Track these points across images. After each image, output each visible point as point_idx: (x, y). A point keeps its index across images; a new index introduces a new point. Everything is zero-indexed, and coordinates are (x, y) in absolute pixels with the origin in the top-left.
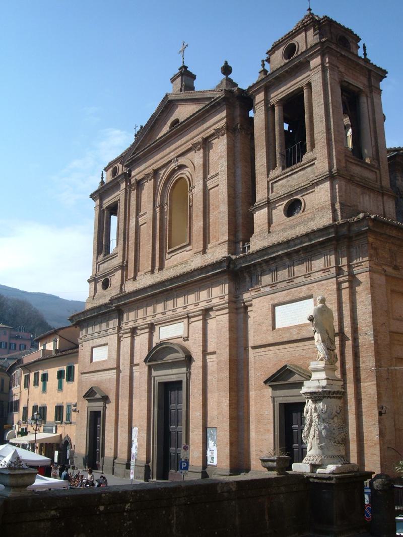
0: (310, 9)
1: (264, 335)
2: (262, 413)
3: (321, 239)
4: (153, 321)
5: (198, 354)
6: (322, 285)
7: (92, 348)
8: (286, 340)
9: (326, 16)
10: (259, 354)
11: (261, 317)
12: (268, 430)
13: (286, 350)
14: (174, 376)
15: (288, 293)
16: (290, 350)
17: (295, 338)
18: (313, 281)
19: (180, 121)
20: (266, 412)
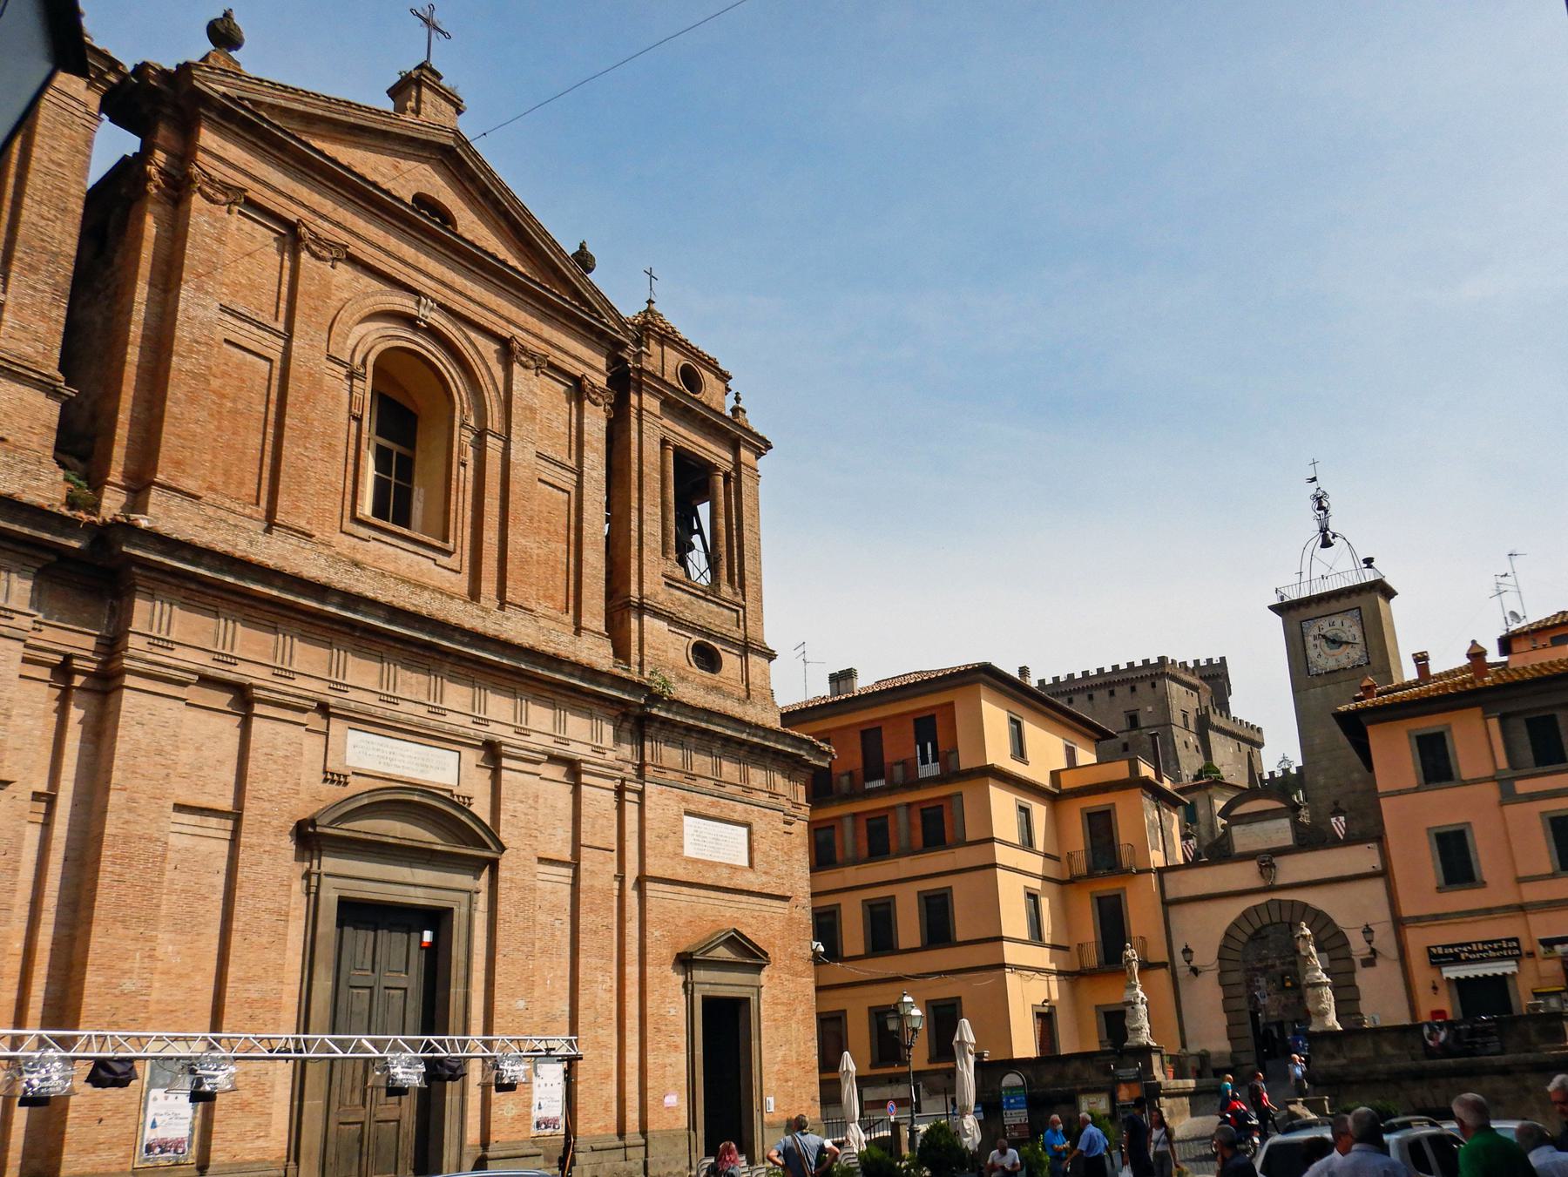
0: (650, 302)
1: (669, 861)
2: (662, 1012)
3: (790, 750)
4: (332, 701)
5: (523, 853)
6: (765, 814)
7: (748, 825)
8: (709, 882)
9: (1259, 730)
10: (660, 894)
11: (663, 825)
12: (676, 1047)
13: (710, 901)
14: (420, 892)
15: (713, 803)
16: (716, 902)
17: (724, 884)
18: (754, 801)
19: (684, 361)
20: (673, 1012)
